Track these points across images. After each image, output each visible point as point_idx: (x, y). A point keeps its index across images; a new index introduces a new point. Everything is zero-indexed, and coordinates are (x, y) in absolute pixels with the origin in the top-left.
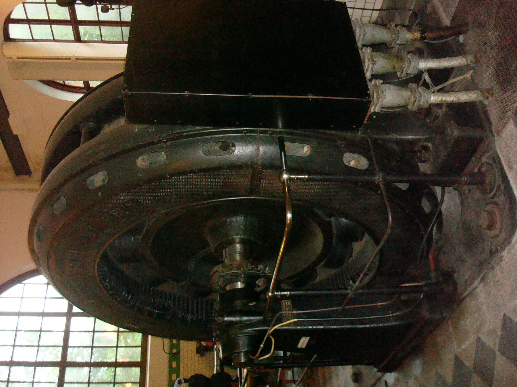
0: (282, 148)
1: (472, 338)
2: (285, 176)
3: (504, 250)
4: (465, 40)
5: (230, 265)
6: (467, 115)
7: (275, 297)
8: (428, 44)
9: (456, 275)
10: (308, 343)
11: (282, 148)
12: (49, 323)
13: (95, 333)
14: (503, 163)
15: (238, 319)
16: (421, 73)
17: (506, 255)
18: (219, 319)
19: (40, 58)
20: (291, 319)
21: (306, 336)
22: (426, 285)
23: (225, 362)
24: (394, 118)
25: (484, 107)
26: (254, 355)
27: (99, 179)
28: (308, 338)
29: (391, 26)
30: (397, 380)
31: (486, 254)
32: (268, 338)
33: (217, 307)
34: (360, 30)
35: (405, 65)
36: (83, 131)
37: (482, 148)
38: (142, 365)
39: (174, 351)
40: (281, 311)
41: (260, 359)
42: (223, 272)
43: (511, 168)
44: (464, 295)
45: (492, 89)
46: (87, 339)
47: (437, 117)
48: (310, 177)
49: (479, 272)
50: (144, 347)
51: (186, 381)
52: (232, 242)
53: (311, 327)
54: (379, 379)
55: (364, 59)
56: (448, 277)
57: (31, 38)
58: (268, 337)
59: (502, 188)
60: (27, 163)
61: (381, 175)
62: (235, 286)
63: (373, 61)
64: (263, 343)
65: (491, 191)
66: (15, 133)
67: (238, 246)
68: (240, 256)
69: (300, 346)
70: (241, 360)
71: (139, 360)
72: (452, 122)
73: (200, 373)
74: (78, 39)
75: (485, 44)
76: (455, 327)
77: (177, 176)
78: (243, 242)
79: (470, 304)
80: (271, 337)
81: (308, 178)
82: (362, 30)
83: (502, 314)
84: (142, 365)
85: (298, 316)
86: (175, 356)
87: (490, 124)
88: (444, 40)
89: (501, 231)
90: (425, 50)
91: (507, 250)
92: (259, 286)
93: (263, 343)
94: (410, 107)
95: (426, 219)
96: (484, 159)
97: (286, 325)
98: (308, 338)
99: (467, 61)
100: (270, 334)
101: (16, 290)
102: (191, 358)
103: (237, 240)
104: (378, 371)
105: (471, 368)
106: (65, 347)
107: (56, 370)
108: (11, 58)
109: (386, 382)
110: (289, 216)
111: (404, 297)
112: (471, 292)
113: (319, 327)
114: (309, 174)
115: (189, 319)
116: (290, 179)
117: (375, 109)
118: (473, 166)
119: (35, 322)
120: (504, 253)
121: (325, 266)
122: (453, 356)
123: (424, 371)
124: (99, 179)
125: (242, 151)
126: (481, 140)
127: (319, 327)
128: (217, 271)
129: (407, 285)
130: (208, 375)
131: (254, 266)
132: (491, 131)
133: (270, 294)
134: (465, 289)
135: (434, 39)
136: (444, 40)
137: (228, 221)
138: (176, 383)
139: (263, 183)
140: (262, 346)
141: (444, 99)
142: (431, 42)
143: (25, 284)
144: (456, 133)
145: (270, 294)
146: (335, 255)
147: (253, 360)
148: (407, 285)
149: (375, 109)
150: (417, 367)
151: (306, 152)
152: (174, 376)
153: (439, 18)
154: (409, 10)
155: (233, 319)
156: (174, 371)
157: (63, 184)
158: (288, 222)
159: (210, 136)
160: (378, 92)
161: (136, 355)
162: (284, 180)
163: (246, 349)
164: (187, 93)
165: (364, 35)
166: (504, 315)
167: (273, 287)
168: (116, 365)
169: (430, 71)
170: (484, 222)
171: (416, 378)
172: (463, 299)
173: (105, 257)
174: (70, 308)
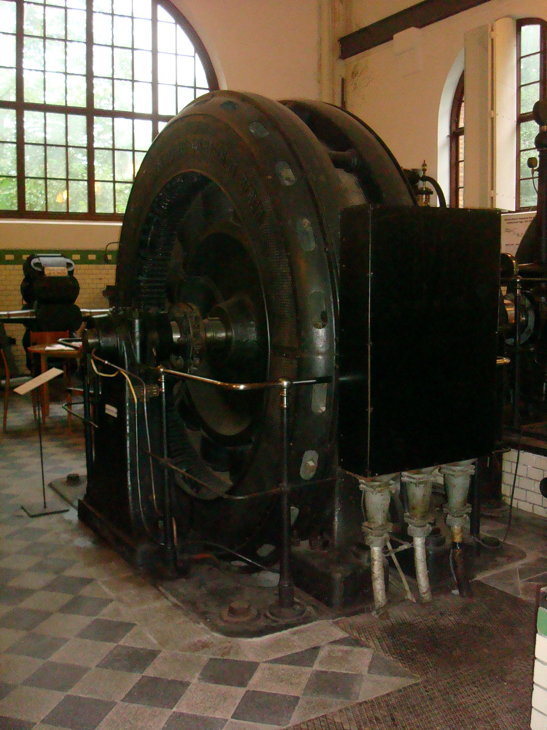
0: (320, 380)
1: (112, 594)
2: (285, 383)
3: (205, 624)
4: (453, 594)
5: (199, 326)
6: (359, 589)
7: (159, 375)
8: (447, 553)
9: (183, 580)
10: (112, 416)
11: (320, 380)
12: (144, 91)
13: (131, 153)
14: (302, 627)
15: (137, 334)
16: (410, 540)
17: (200, 626)
18: (136, 312)
19: (492, 67)
20: (137, 396)
21: (118, 413)
22: (173, 546)
23: (90, 321)
24: (357, 510)
25: (369, 611)
26: (97, 353)
27: (288, 175)
28: (116, 416)
29: (467, 508)
30: (70, 522)
31: (202, 607)
32: (115, 370)
33: (153, 311)
34: (459, 471)
35: (417, 521)
36: (347, 153)
37: (322, 607)
38: (91, 214)
39: (110, 257)
40: (146, 384)
41: (92, 361)
42: (191, 317)
43: (294, 633)
44: (160, 588)
45: (388, 618)
46: (123, 142)
47: (357, 556)
48: (285, 410)
49: (183, 602)
50: (112, 217)
51: (71, 273)
52: (227, 329)
53: (128, 417)
54: (71, 504)
55: (422, 473)
56: (183, 572)
57: (522, 55)
58: (116, 370)
59: (274, 624)
60: (356, 54)
61: (288, 489)
62: (176, 333)
63: (420, 483)
64: (109, 364)
65: (272, 614)
66: (395, 36)
67: (223, 335)
68: (211, 336)
69: (108, 407)
70: (91, 339)
71: (98, 211)
72: (349, 574)
73: (81, 291)
74: (522, 119)
75: (441, 614)
76: (128, 580)
77: (289, 263)
78: (228, 340)
79: (149, 593)
80: (117, 373)
81: (283, 408)
82: (459, 473)
83: (136, 623)
84: (91, 214)
85: (141, 404)
86: (102, 257)
87: (348, 615)
88: (453, 571)
89: (226, 622)
90: (442, 548)
91: (207, 628)
92: (177, 359)
93: (109, 364)
94: (366, 524)
95: (252, 553)
96: (309, 609)
97: (130, 390)
98: (116, 416)
99: (424, 593)
100: (119, 372)
101: (187, 46)
102: (101, 279)
103: (230, 334)
104: (79, 500)
105: (80, 593)
106: (113, 114)
107: (82, 103)
108: (492, 30)
109: (68, 511)
110: (242, 387)
111: (161, 523)
112: (163, 594)
113: (128, 427)
114: (287, 409)
115: (140, 278)
116: (282, 388)
117: (363, 483)
118: (300, 597)
119: (144, 73)
120: (202, 625)
121: (204, 439)
122: (95, 577)
123: (78, 549)
124: (288, 175)
125: (320, 336)
126: (329, 604)
127: (128, 427)
128: (193, 310)
129: (175, 528)
130: (78, 302)
131: (198, 353)
132: (339, 616)
133: (162, 370)
134: (167, 589)
135: (453, 559)
136: (453, 571)
137: (252, 323)
138: (68, 261)
139: (284, 361)
140: (106, 362)
141: (376, 563)
142: (451, 555)
143: (194, 57)
144: (338, 576)
145: (162, 370)
146: (215, 449)
147: (90, 353)
148: (175, 528)
149: (363, 483)
150: (84, 542)
151: (320, 410)
152: (77, 257)
153: (487, 569)
154: (505, 540)
155: (137, 329)
156: (84, 256)
157: (282, 134)
158: (234, 386)
159: (332, 299)
160: (379, 486)
161: (103, 207)
162: (280, 382)
163: (102, 344)
164: (370, 274)
165: (453, 476)
166: (135, 624)
167: (170, 373)
168: (91, 180)
169: (411, 552)
170: (236, 605)
171: (72, 541)
172: (156, 587)
173: (204, 181)
174: (165, 119)
